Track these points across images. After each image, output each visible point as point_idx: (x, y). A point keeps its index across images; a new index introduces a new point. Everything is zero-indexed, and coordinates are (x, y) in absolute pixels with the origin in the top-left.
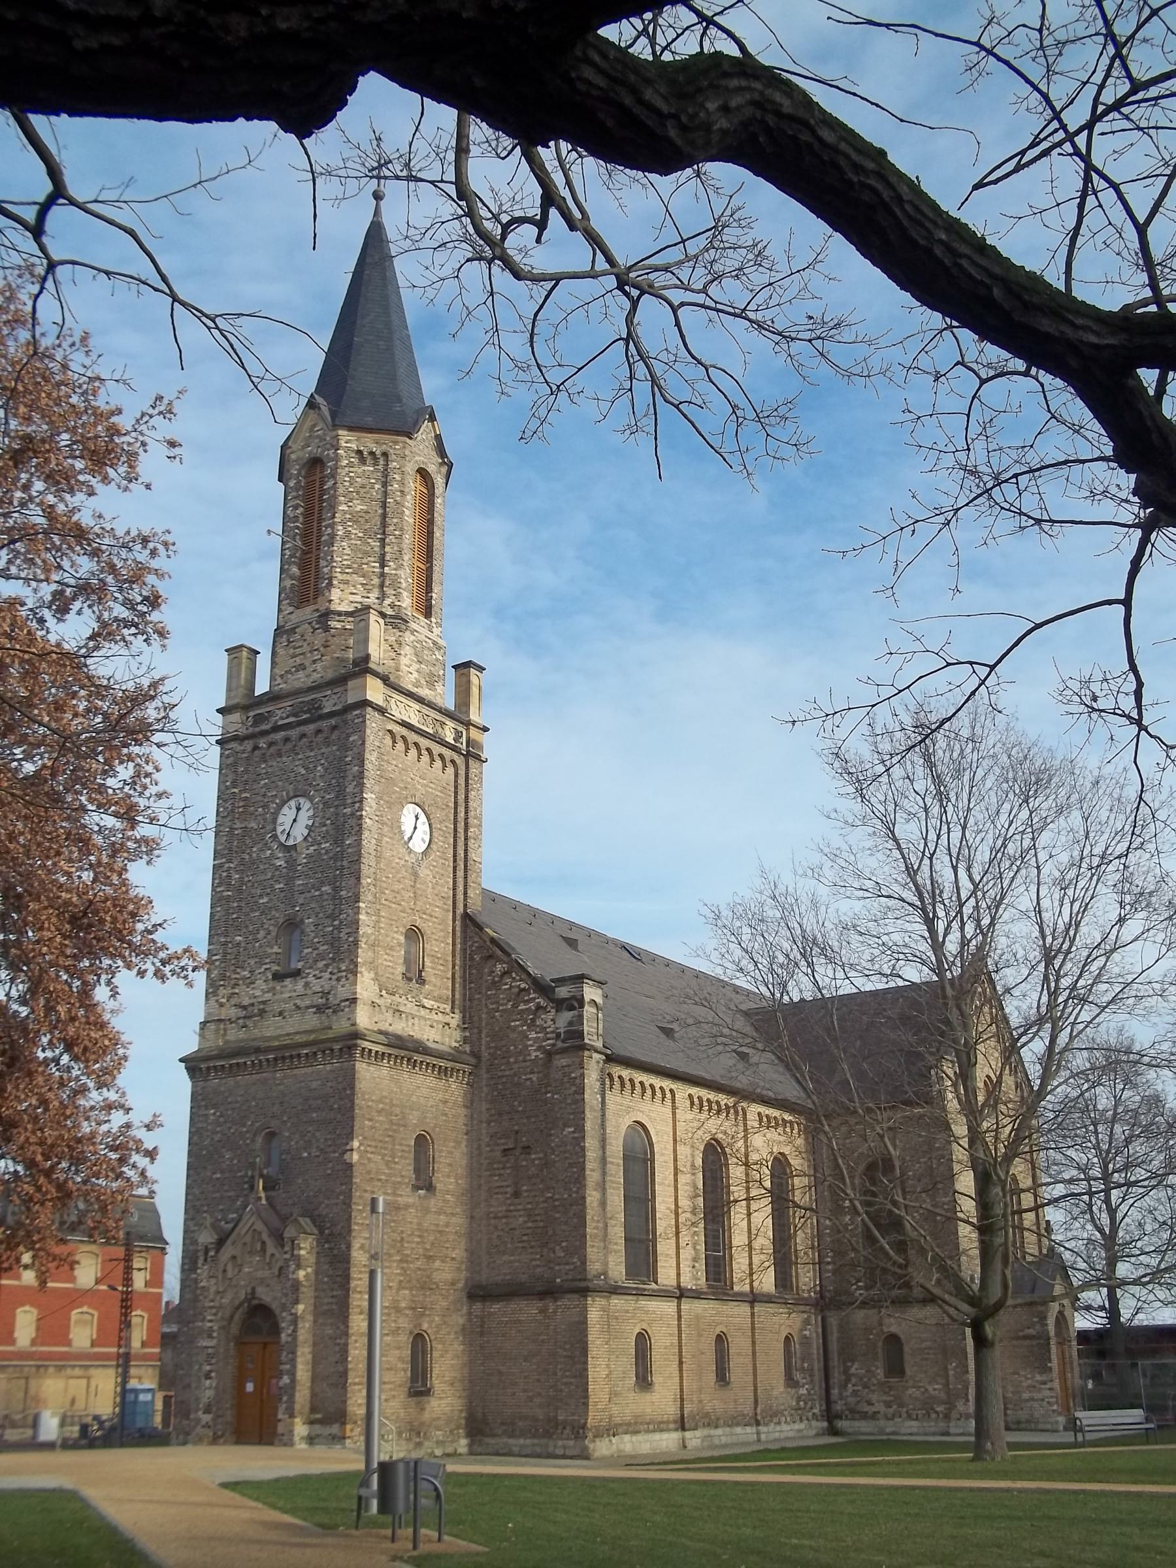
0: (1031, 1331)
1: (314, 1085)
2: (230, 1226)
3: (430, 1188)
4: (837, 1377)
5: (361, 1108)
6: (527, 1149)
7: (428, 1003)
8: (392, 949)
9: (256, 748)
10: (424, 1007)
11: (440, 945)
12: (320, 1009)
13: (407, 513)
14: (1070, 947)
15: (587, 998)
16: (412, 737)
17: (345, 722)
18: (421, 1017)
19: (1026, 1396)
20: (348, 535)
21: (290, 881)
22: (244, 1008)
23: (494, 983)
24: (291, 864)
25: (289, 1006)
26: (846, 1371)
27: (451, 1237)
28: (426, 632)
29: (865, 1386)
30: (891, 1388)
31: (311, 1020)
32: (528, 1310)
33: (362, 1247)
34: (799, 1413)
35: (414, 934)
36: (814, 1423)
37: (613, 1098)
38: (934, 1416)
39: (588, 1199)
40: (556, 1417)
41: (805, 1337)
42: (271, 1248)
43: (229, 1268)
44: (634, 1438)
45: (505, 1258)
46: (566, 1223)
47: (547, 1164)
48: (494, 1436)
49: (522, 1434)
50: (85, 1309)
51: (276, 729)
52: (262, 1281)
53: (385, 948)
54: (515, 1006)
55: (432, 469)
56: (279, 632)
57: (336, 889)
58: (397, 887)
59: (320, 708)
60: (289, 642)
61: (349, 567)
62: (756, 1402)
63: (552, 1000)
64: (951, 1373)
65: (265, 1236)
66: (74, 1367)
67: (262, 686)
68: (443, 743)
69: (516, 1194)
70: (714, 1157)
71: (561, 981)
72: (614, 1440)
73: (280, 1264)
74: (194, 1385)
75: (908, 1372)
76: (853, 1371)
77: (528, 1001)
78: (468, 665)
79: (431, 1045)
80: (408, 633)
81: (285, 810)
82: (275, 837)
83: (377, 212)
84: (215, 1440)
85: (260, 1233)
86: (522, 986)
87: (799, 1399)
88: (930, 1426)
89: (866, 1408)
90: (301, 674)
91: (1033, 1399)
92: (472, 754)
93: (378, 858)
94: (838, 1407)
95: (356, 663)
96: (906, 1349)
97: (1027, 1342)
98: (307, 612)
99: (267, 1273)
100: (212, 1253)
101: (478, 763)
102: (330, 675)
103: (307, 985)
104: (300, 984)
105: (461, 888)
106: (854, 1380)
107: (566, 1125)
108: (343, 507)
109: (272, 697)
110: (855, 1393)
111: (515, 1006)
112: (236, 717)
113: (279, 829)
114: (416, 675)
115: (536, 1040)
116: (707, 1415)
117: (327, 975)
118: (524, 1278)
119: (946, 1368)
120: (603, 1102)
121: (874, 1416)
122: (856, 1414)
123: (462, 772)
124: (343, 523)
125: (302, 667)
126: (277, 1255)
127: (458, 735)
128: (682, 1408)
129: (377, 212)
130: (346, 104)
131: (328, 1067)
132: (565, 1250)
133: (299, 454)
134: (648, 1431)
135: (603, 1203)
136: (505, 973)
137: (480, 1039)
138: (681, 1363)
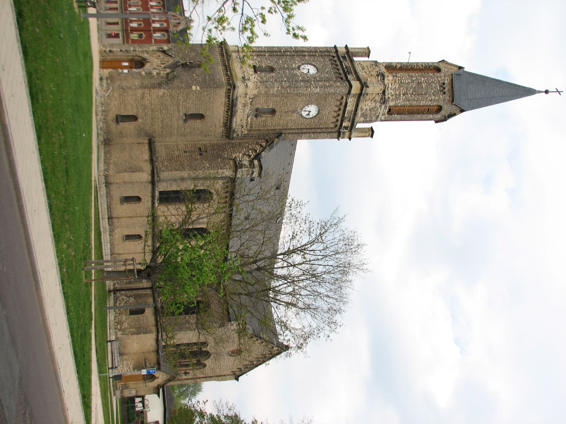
1: (218, 77)
3: (185, 121)
4: (129, 293)
5: (210, 90)
6: (201, 154)
8: (267, 103)
9: (334, 57)
10: (248, 117)
11: (271, 123)
12: (244, 78)
13: (424, 102)
14: (251, 201)
19: (125, 362)
21: (288, 69)
24: (294, 69)
25: (244, 70)
26: (131, 296)
27: (170, 130)
30: (125, 311)
31: (240, 75)
32: (146, 156)
35: (273, 112)
39: (184, 172)
42: (163, 66)
44: (105, 195)
48: (105, 148)
49: (105, 156)
51: (341, 63)
52: (152, 64)
53: (266, 100)
54: (250, 149)
55: (443, 112)
56: (376, 62)
57: (285, 81)
59: (349, 74)
61: (401, 82)
62: (119, 254)
65: (167, 64)
67: (355, 59)
68: (342, 122)
69: (185, 152)
72: (104, 185)
75: (131, 316)
76: (131, 298)
77: (252, 152)
80: (379, 104)
81: (314, 115)
82: (303, 64)
83: (540, 92)
88: (112, 323)
90: (361, 69)
91: (123, 365)
93: (297, 94)
94: (118, 294)
97: (144, 363)
98: (383, 70)
101: (336, 136)
102: (361, 77)
103: (252, 75)
105: (291, 131)
106: (128, 299)
109: (352, 61)
110: (124, 299)
111: (250, 149)
112: (344, 50)
113: (306, 65)
114: (365, 108)
116: (114, 231)
117: (255, 80)
122: (116, 299)
124: (417, 79)
125: (363, 69)
127: (346, 128)
128: (116, 218)
129: (540, 92)
134: (107, 202)
136: (262, 146)
137: (238, 139)
138: (131, 217)
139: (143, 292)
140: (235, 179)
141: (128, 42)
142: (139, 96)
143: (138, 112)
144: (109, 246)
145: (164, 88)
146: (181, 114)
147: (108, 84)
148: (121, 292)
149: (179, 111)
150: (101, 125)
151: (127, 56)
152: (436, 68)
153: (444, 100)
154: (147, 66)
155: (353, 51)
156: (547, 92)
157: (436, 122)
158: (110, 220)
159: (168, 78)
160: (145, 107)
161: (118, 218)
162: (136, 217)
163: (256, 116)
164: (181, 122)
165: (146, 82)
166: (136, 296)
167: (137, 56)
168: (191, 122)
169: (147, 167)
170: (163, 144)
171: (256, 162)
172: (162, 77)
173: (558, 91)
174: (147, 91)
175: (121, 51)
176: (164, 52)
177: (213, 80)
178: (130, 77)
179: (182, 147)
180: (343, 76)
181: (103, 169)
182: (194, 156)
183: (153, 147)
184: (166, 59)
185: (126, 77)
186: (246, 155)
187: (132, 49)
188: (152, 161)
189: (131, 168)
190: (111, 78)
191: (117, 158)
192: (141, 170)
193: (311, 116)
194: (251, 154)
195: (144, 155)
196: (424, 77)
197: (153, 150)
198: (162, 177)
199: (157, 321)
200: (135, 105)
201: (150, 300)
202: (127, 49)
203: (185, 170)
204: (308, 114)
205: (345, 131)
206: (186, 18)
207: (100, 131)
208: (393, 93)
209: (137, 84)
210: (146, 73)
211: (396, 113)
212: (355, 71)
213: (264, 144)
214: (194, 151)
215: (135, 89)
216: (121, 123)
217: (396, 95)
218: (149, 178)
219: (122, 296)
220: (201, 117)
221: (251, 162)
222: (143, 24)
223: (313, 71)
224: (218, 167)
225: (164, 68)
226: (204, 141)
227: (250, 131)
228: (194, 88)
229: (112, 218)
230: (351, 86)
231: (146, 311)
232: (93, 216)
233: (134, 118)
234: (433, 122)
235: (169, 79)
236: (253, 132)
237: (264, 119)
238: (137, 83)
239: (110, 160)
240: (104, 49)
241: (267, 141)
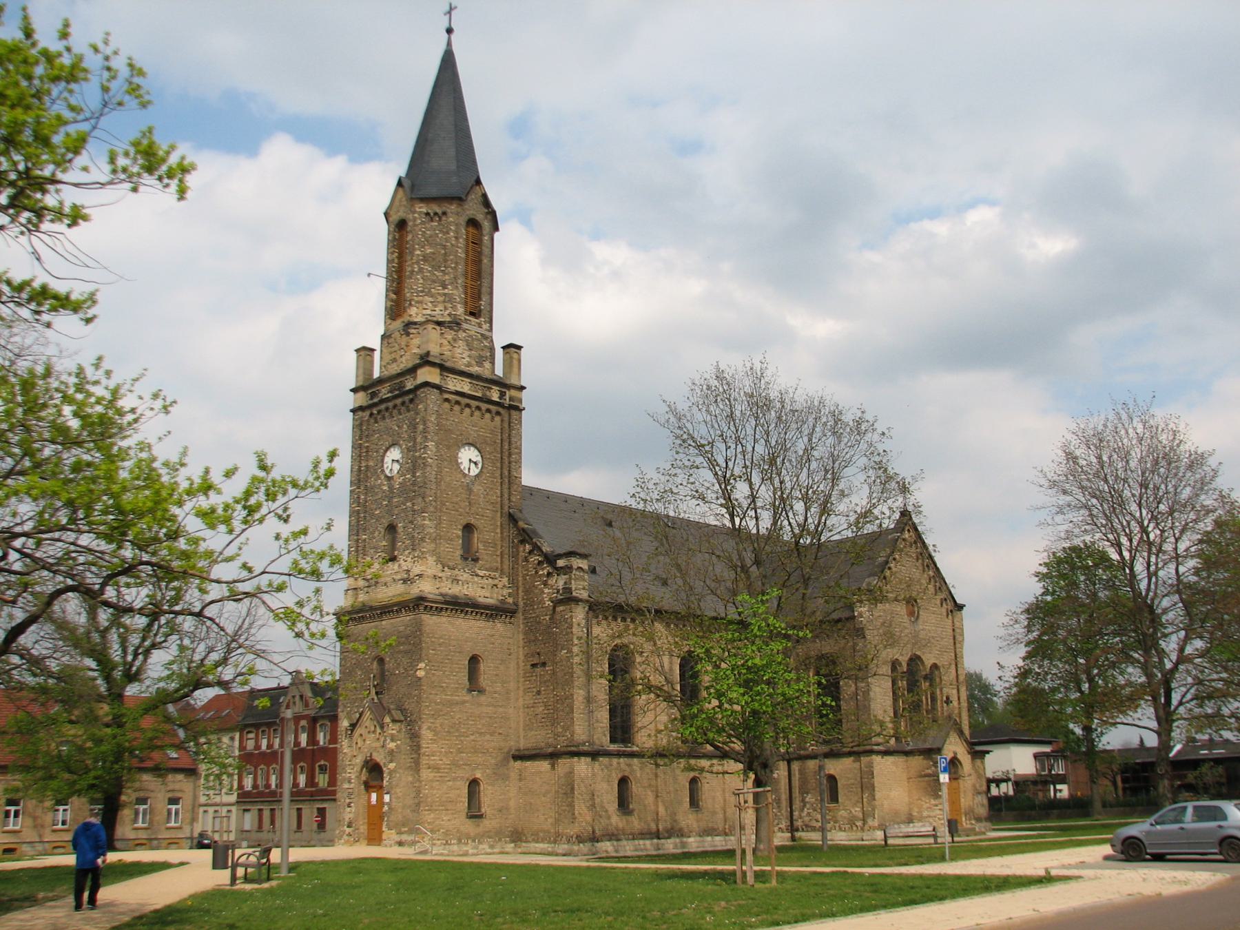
0: (929, 771)
3: (481, 691)
4: (797, 804)
6: (544, 664)
7: (481, 573)
9: (371, 415)
12: (405, 581)
15: (575, 567)
16: (465, 401)
18: (474, 583)
19: (925, 814)
20: (421, 270)
22: (367, 580)
24: (391, 488)
26: (803, 801)
32: (544, 765)
48: (527, 841)
49: (542, 841)
51: (382, 401)
55: (480, 217)
56: (383, 337)
58: (455, 500)
69: (539, 693)
71: (560, 556)
78: (511, 346)
79: (481, 600)
81: (476, 452)
82: (383, 471)
83: (449, 44)
90: (394, 365)
92: (516, 408)
93: (438, 483)
94: (799, 823)
95: (422, 357)
96: (839, 785)
104: (396, 565)
108: (418, 252)
109: (381, 381)
110: (809, 814)
123: (506, 419)
125: (394, 360)
127: (502, 395)
129: (449, 44)
132: (563, 727)
133: (395, 218)
146: (468, 698)
149: (464, 702)
152: (399, 227)
153: (457, 214)
155: (361, 378)
156: (449, 31)
157: (496, 228)
160: (455, 764)
163: (476, 560)
164: (483, 698)
166: (804, 791)
168: (483, 681)
174: (424, 761)
177: (407, 637)
180: (407, 398)
181: (566, 846)
183: (527, 753)
193: (479, 459)
199: (850, 754)
204: (476, 463)
205: (507, 397)
211: (478, 299)
220: (474, 660)
222: (302, 764)
223: (395, 454)
231: (832, 772)
233: (474, 784)
234: (496, 235)
237: (481, 547)
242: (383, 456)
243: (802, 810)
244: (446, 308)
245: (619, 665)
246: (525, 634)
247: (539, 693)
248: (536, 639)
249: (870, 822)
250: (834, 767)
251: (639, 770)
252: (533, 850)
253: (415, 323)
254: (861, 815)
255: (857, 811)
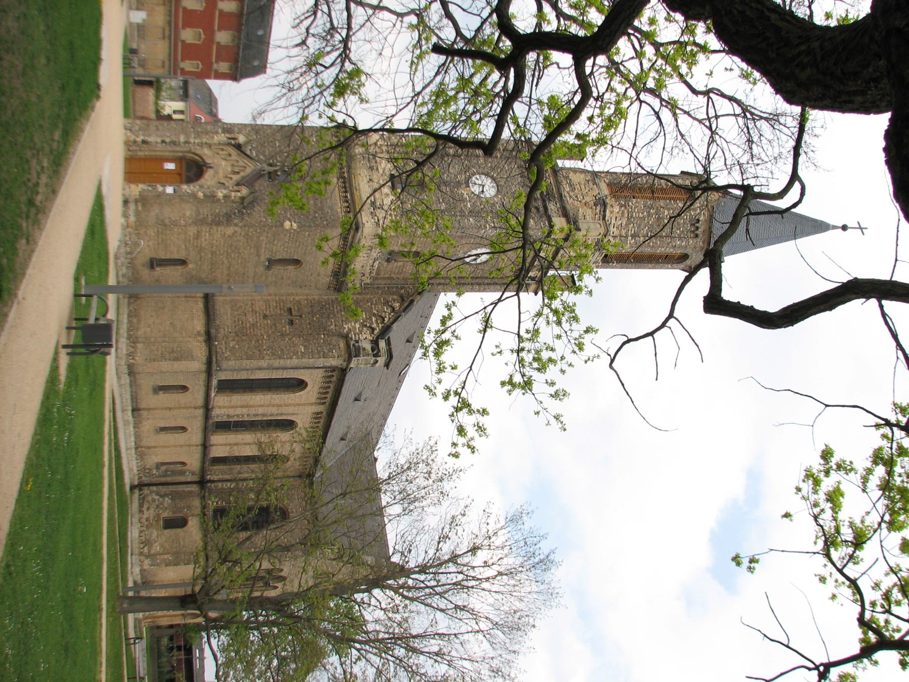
2: (248, 153)
3: (268, 268)
4: (163, 489)
6: (291, 323)
17: (541, 217)
23: (388, 302)
28: (594, 260)
29: (158, 506)
30: (157, 521)
32: (199, 325)
33: (236, 232)
34: (143, 470)
36: (137, 478)
37: (320, 373)
38: (142, 546)
40: (139, 342)
41: (185, 473)
42: (236, 178)
43: (225, 152)
45: (229, 310)
46: (249, 348)
47: (283, 335)
48: (129, 304)
49: (130, 322)
50: (203, 36)
52: (217, 173)
54: (374, 315)
60: (588, 181)
63: (378, 338)
64: (166, 556)
65: (242, 174)
66: (170, 31)
69: (265, 317)
70: (288, 425)
71: (388, 343)
73: (227, 184)
74: (158, 133)
76: (167, 499)
83: (835, 227)
84: (128, 144)
85: (244, 171)
86: (386, 319)
87: (150, 469)
89: (146, 506)
94: (146, 491)
96: (179, 530)
99: (221, 174)
100: (233, 142)
102: (568, 207)
103: (387, 195)
106: (161, 499)
107: (305, 346)
110: (154, 500)
111: (374, 315)
115: (355, 328)
116: (140, 422)
118: (218, 322)
119: (168, 553)
120: (318, 368)
121: (141, 511)
122: (142, 500)
126: (231, 182)
127: (533, 279)
128: (144, 409)
129: (835, 227)
130: (856, 279)
131: (339, 210)
132: (234, 347)
134: (132, 392)
135: (260, 369)
136: (393, 309)
138: (170, 409)
139: (187, 488)
140: (345, 370)
141: (175, 73)
142: (192, 234)
143: (188, 255)
144: (133, 439)
145: (236, 225)
146: (263, 259)
147: (137, 213)
148: (151, 488)
149: (259, 256)
150: (124, 270)
151: (174, 151)
153: (695, 247)
154: (209, 178)
156: (844, 228)
158: (136, 413)
159: (242, 203)
160: (201, 250)
161: (149, 409)
162: (180, 408)
163: (388, 261)
164: (261, 269)
165: (205, 211)
166: (175, 496)
167: (190, 152)
168: (278, 269)
169: (200, 350)
170: (228, 298)
171: (382, 344)
172: (233, 202)
173: (861, 228)
174: (205, 229)
175: (163, 142)
176: (238, 147)
177: (321, 209)
178: (177, 200)
179: (260, 306)
181: (125, 352)
182: (279, 326)
183: (211, 304)
184: (241, 163)
185: (170, 200)
186: (366, 326)
187: (182, 139)
188: (209, 338)
189: (173, 352)
190: (143, 200)
191: (149, 326)
192: (190, 357)
194: (374, 325)
195: (196, 322)
196: (669, 210)
197: (211, 313)
198: (224, 366)
200: (183, 246)
201: (197, 503)
202: (174, 138)
203: (263, 358)
205: (530, 282)
206: (287, 230)
207: (121, 279)
208: (616, 233)
209: (188, 213)
210: (205, 196)
212: (561, 196)
213: (397, 305)
214: (281, 314)
215: (185, 226)
216: (158, 269)
217: (621, 236)
218: (204, 368)
219: (152, 494)
220: (297, 262)
221: (375, 343)
222: (201, 66)
223: (490, 190)
224: (319, 352)
225: (238, 184)
226: (297, 295)
227: (375, 279)
228: (287, 224)
229: (139, 410)
230: (551, 226)
231: (190, 523)
232: (107, 463)
233: (183, 262)
235: (245, 204)
236: (380, 281)
237: (399, 264)
238: (189, 211)
239: (138, 329)
240: (133, 138)
241: (402, 299)
242: (487, 175)
243: (157, 494)
244: (614, 237)
245: (288, 425)
246: (319, 302)
247: (265, 317)
248: (314, 315)
249: (147, 562)
250: (193, 524)
251: (196, 396)
252: (121, 311)
253: (605, 211)
254: (153, 552)
255: (156, 548)
